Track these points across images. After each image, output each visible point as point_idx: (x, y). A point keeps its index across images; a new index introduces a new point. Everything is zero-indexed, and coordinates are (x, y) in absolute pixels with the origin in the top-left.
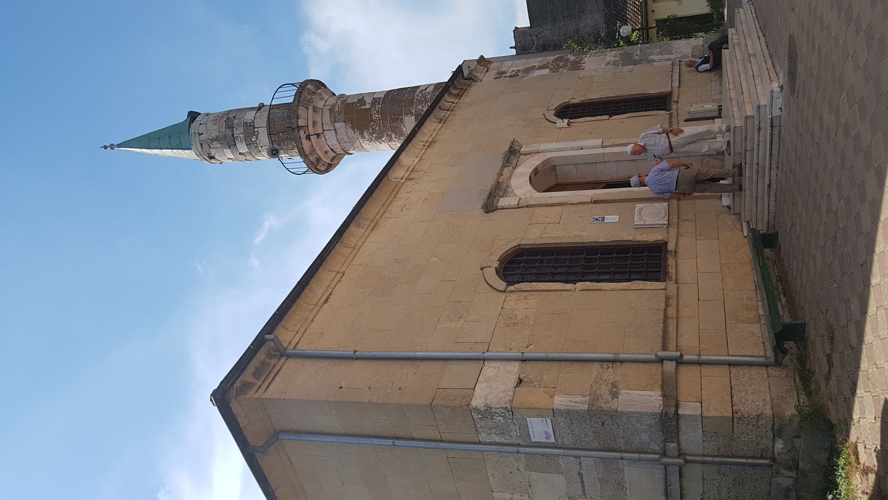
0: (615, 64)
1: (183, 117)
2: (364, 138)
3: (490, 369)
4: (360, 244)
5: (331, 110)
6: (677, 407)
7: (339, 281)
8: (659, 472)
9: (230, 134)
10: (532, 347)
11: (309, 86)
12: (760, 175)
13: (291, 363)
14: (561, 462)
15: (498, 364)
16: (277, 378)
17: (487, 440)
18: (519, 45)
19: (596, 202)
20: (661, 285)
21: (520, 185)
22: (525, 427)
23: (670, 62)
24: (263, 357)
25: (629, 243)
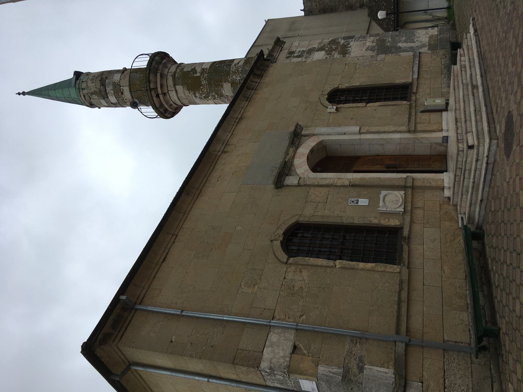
0: (371, 49)
1: (71, 76)
2: (196, 97)
7: (174, 242)
10: (304, 317)
12: (474, 190)
18: (307, 9)
20: (396, 268)
21: (301, 165)
23: (411, 54)
25: (375, 226)
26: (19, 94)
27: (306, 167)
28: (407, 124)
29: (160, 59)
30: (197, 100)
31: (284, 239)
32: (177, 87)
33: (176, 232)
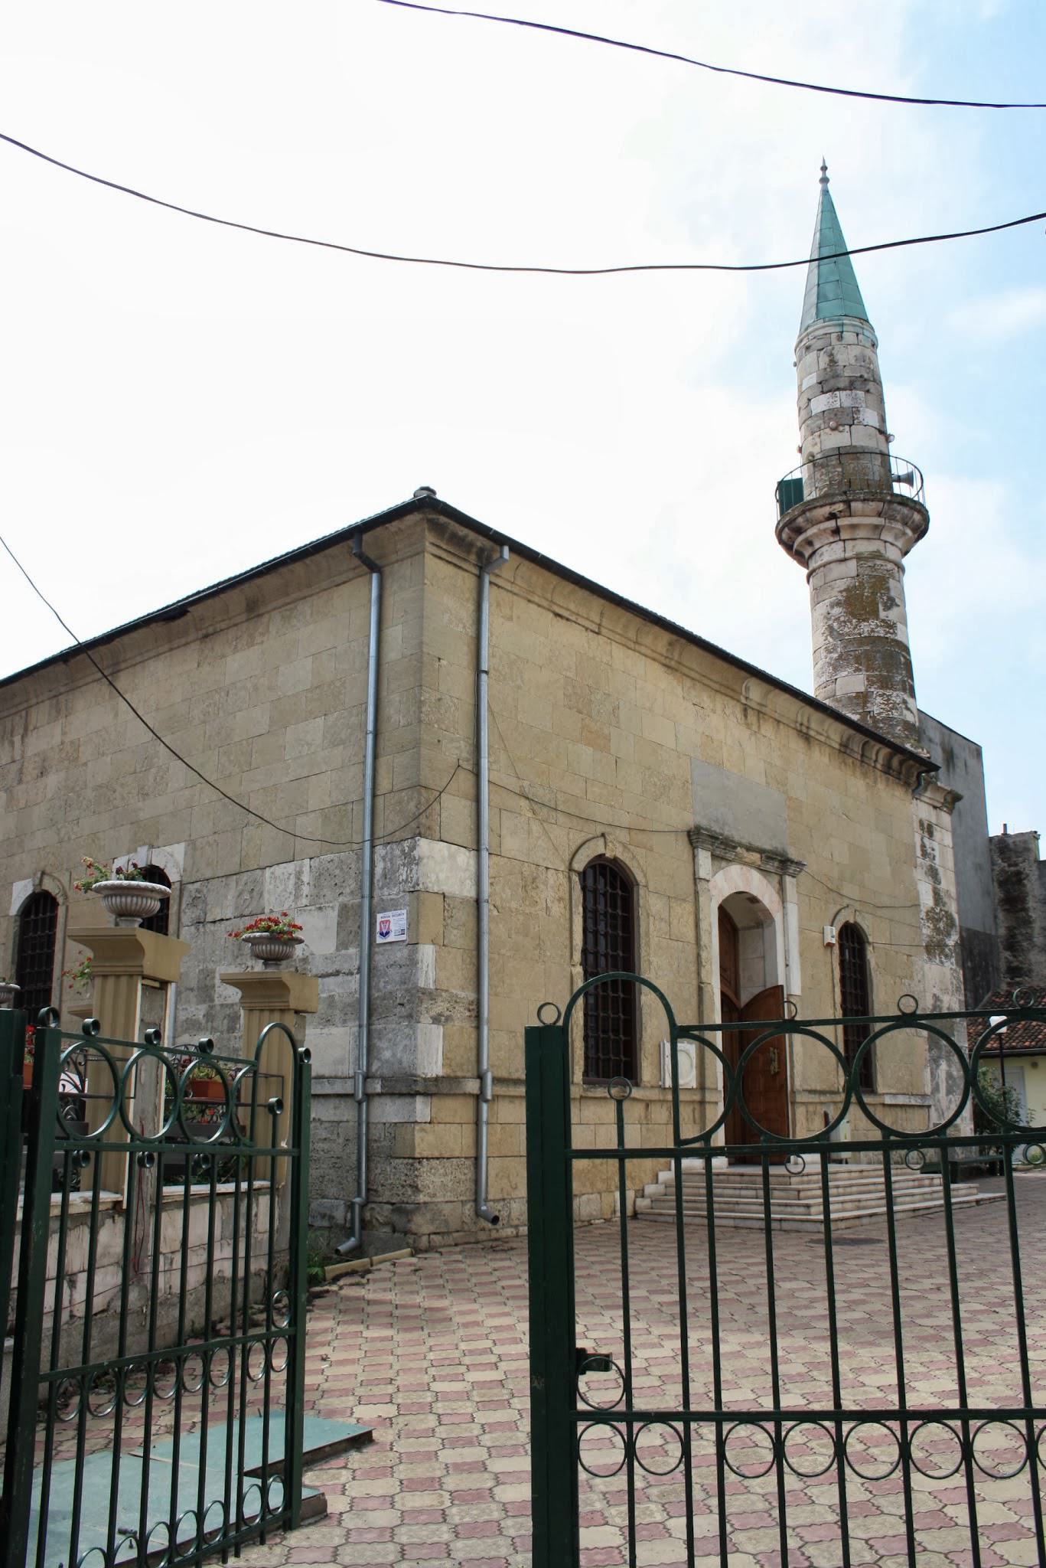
2: (832, 607)
3: (465, 858)
4: (643, 650)
5: (877, 555)
6: (425, 1094)
8: (348, 1069)
9: (841, 385)
10: (495, 913)
11: (917, 517)
13: (470, 581)
14: (352, 951)
15: (473, 869)
16: (451, 568)
17: (377, 857)
18: (1010, 841)
19: (700, 990)
22: (395, 905)
23: (928, 1090)
24: (479, 544)
26: (824, 168)
27: (727, 891)
28: (806, 1087)
29: (915, 521)
30: (822, 608)
31: (607, 859)
32: (853, 564)
33: (604, 631)
